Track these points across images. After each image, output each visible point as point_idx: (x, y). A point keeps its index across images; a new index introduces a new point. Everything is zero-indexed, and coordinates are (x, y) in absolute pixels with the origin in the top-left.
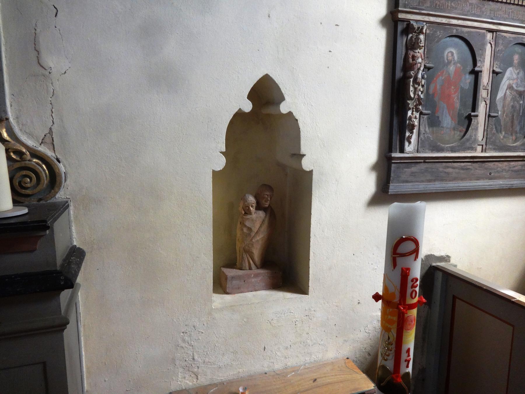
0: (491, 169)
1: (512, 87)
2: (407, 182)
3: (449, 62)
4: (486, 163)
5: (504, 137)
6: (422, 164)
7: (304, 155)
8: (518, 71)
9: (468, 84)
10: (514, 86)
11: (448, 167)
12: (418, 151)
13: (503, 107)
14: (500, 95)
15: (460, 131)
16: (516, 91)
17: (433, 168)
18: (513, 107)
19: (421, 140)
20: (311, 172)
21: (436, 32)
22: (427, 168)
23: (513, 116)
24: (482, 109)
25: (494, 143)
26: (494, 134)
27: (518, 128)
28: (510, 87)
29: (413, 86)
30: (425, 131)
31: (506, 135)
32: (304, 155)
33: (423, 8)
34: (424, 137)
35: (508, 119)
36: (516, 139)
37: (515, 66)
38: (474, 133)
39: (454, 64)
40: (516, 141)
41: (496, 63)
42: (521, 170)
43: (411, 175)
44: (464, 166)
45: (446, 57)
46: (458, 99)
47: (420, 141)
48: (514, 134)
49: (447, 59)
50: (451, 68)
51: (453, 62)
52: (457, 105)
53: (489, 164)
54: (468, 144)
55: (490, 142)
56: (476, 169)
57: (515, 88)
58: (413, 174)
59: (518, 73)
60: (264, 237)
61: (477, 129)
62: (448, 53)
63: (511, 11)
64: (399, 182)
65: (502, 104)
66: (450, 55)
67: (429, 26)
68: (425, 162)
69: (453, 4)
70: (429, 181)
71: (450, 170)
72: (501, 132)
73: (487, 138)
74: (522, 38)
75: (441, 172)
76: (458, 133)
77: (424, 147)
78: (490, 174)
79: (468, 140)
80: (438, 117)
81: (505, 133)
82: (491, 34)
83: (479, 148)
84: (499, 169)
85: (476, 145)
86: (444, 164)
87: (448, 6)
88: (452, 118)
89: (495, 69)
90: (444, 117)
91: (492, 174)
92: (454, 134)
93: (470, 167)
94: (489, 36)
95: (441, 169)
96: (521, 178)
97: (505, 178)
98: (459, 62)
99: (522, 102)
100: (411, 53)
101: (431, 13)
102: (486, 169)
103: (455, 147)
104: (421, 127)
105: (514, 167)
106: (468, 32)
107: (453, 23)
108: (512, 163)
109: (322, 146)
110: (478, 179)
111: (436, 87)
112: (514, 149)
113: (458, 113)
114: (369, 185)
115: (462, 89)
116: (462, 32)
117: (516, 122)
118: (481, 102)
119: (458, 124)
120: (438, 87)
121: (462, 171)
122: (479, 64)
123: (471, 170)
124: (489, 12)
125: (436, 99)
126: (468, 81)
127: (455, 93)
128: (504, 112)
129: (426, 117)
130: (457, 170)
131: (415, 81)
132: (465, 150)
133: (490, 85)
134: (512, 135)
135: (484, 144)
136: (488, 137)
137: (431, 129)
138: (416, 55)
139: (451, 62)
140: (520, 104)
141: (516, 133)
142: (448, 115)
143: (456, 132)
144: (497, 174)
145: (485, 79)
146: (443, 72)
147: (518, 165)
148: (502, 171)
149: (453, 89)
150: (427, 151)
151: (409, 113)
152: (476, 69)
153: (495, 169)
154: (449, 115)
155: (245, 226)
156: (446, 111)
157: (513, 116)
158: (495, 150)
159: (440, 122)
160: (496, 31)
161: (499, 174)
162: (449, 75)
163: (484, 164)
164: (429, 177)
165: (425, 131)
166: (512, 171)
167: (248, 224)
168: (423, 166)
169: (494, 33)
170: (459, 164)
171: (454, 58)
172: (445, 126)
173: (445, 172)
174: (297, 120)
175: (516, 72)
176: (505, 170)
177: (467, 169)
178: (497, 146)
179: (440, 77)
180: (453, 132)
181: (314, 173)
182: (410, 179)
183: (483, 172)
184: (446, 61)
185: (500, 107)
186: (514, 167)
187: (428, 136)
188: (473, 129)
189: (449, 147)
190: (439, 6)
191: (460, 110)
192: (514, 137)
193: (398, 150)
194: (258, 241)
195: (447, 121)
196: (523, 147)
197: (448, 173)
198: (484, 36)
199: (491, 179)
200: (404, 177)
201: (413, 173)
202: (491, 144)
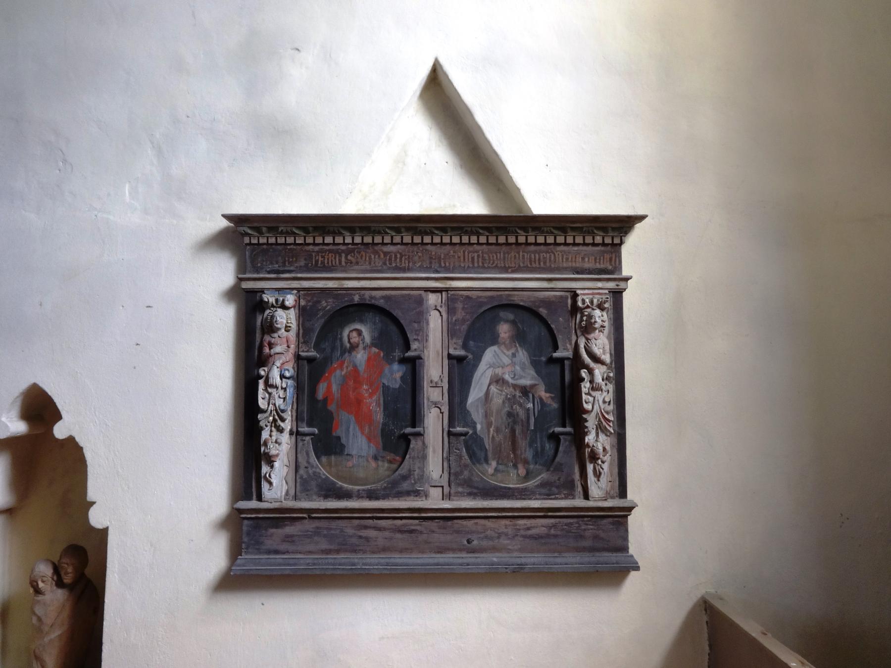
0: (472, 532)
1: (503, 380)
2: (277, 552)
3: (353, 347)
4: (456, 521)
5: (496, 470)
6: (306, 521)
7: (94, 503)
8: (513, 351)
9: (398, 379)
10: (507, 377)
11: (366, 527)
12: (296, 498)
13: (486, 415)
14: (475, 394)
15: (390, 462)
16: (515, 386)
17: (331, 529)
18: (510, 414)
19: (301, 477)
20: (104, 532)
21: (319, 302)
22: (318, 528)
23: (513, 431)
24: (434, 423)
25: (468, 483)
26: (466, 466)
27: (529, 454)
28: (498, 380)
29: (266, 390)
30: (308, 462)
31: (501, 467)
32: (94, 503)
33: (292, 268)
34: (307, 472)
35: (501, 437)
36: (527, 473)
37: (504, 343)
38: (418, 465)
39: (364, 348)
40: (528, 476)
41: (454, 340)
42: (548, 536)
43: (284, 541)
44: (404, 525)
45: (345, 339)
46: (378, 405)
47: (298, 480)
48: (520, 466)
49: (349, 342)
50: (359, 356)
51: (361, 346)
52: (379, 417)
53: (464, 522)
54: (405, 486)
55: (460, 480)
56: (433, 532)
57: (510, 381)
58: (289, 539)
59: (514, 355)
60: (60, 636)
61: (424, 457)
62: (351, 331)
63: (476, 255)
64: (259, 552)
65: (481, 411)
66: (354, 334)
67: (304, 295)
68: (310, 518)
69: (349, 257)
70: (328, 552)
71: (372, 533)
72: (486, 461)
73: (450, 473)
74: (509, 295)
75: (351, 537)
76: (386, 465)
77: (308, 490)
78: (469, 542)
79: (405, 478)
80: (339, 438)
81: (498, 463)
82: (439, 294)
83: (435, 493)
84: (489, 532)
85: (427, 485)
86: (356, 522)
87: (317, 261)
88: (369, 439)
89: (452, 352)
90: (351, 438)
91: (475, 542)
92: (377, 468)
93: (418, 528)
94: (433, 299)
95: (350, 531)
96: (550, 551)
97: (509, 551)
98: (373, 344)
99: (530, 405)
100: (267, 338)
101: (299, 275)
102: (458, 532)
103: (378, 490)
104: (299, 455)
105: (528, 529)
106: (383, 297)
107: (349, 286)
108: (521, 522)
109: (126, 488)
110: (441, 550)
111: (329, 387)
112: (522, 494)
113: (383, 430)
114: (215, 556)
115: (386, 388)
116: (371, 298)
117: (522, 443)
118: (429, 409)
119: (385, 448)
120: (334, 388)
121: (399, 536)
122: (414, 345)
123: (421, 533)
124: (428, 262)
125: (332, 407)
126: (398, 375)
127: (371, 395)
128: (489, 425)
129: (308, 438)
130: (387, 534)
131: (268, 385)
132: (399, 495)
133: (446, 380)
134: (515, 466)
135: (446, 485)
136: (452, 471)
137: (324, 459)
138: (273, 340)
139: (357, 346)
140: (528, 410)
141: (526, 462)
142: (359, 434)
143: (380, 463)
144: (485, 543)
145: (435, 369)
146: (343, 363)
147: (540, 525)
148: (499, 538)
149: (366, 390)
150: (314, 497)
151: (265, 435)
152: (410, 354)
153: (478, 533)
154: (363, 433)
155: (34, 613)
156: (354, 428)
157: (513, 431)
158: (472, 495)
159: (343, 447)
160: (447, 290)
161: (491, 543)
162: (355, 367)
163: (449, 523)
164: (324, 545)
165: (308, 462)
166: (525, 537)
167: (39, 610)
168: (309, 525)
169: (444, 293)
170: (390, 522)
171: (363, 340)
172: (354, 452)
173: (360, 537)
174: (82, 448)
175: (510, 353)
176: (506, 535)
177: (411, 532)
178: (477, 488)
179: (338, 372)
180: (373, 464)
181: (110, 532)
182: (283, 547)
183: (449, 538)
184: (348, 345)
185: (477, 416)
186: (528, 529)
187: (314, 473)
188: (413, 458)
189: (364, 490)
190: (323, 263)
191: (384, 424)
192: (522, 471)
193: (254, 496)
194: (51, 640)
195: (359, 444)
196: (543, 491)
197: (367, 539)
198: (420, 301)
199: (473, 551)
200: (269, 543)
201: (287, 536)
202: (459, 485)
